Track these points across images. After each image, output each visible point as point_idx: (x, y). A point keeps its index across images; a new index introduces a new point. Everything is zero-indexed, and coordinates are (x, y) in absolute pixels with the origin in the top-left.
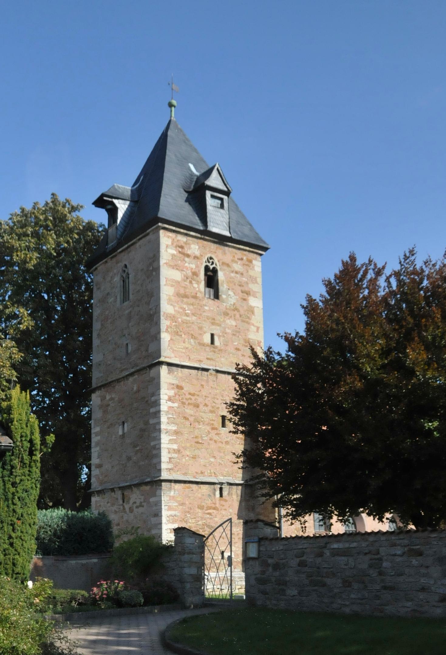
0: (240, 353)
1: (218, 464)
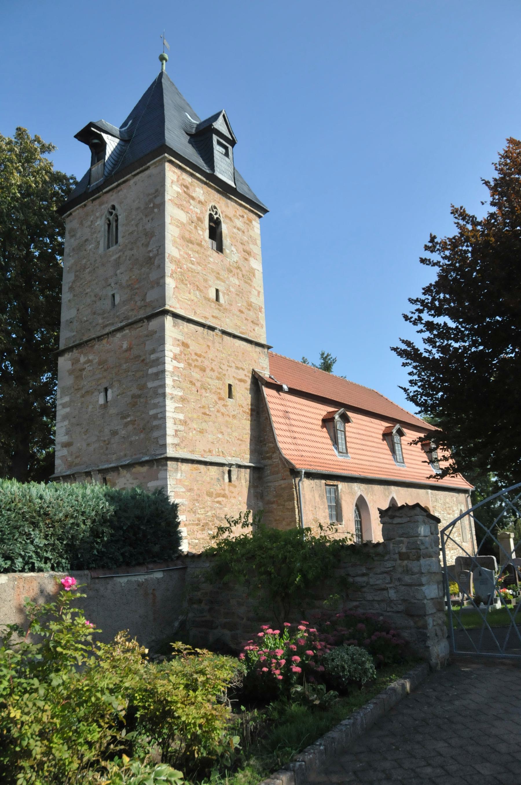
0: (243, 316)
1: (226, 441)
